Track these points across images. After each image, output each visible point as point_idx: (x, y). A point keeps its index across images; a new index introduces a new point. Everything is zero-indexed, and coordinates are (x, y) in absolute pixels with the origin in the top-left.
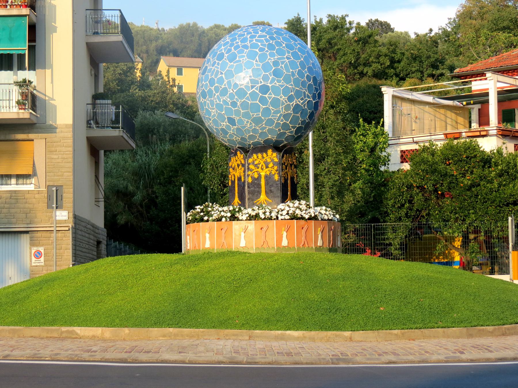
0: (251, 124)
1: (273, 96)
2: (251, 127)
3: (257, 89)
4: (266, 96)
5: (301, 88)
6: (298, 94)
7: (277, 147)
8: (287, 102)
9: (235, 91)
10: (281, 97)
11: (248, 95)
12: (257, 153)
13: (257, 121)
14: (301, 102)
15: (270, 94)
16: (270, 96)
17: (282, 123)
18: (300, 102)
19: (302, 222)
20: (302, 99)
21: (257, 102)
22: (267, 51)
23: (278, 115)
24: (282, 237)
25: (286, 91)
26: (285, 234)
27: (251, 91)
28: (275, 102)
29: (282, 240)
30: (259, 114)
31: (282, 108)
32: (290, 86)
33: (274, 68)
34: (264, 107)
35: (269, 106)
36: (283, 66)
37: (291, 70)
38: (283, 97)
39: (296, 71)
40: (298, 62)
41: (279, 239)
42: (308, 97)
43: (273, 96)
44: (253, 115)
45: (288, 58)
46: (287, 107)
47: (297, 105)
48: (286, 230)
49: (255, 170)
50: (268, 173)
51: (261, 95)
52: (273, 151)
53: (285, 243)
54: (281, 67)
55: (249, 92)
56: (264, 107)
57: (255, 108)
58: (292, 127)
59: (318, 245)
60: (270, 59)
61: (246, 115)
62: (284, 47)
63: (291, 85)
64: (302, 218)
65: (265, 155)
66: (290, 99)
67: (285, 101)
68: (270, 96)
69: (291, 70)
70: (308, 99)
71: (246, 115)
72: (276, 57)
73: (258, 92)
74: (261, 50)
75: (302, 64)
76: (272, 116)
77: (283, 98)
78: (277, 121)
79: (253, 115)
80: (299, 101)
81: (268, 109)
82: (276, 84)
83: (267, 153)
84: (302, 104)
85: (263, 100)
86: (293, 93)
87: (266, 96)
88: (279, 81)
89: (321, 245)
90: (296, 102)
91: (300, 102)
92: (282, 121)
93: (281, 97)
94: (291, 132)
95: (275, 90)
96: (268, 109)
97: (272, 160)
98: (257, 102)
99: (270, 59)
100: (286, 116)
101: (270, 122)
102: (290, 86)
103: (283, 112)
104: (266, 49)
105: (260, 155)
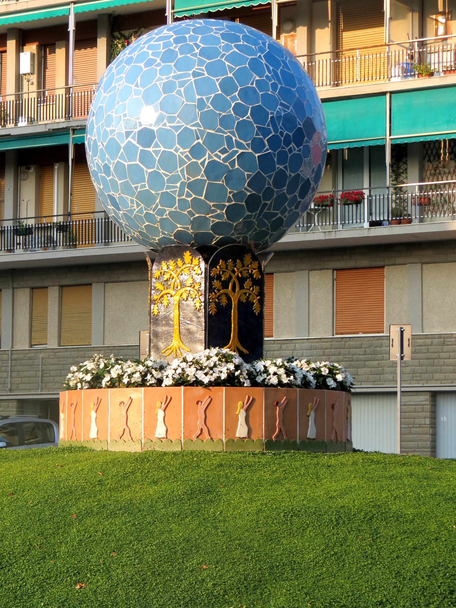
0: (138, 205)
1: (162, 149)
2: (140, 211)
3: (133, 138)
4: (150, 149)
5: (219, 130)
6: (212, 142)
7: (204, 250)
8: (189, 159)
9: (105, 144)
10: (177, 150)
11: (122, 150)
12: (167, 259)
13: (146, 198)
14: (223, 156)
15: (157, 146)
16: (156, 149)
17: (189, 199)
18: (219, 157)
19: (199, 390)
20: (223, 151)
21: (138, 162)
22: (159, 65)
23: (178, 185)
24: (156, 420)
25: (185, 137)
26: (160, 414)
27: (126, 142)
28: (168, 160)
29: (155, 427)
30: (144, 186)
31: (182, 171)
32: (194, 128)
33: (164, 95)
34: (149, 171)
35: (158, 168)
36: (182, 89)
37: (198, 97)
38: (181, 150)
39: (208, 99)
40: (217, 81)
41: (150, 426)
42: (240, 146)
43: (162, 149)
44: (136, 188)
45: (195, 74)
46: (193, 169)
47: (213, 164)
48: (163, 406)
49: (164, 292)
50: (244, 300)
51: (141, 148)
52: (193, 255)
53: (160, 431)
54: (179, 92)
55: (123, 145)
56: (149, 171)
57: (136, 174)
58: (213, 205)
59: (237, 435)
60: (159, 79)
61: (126, 188)
62: (195, 55)
63: (197, 125)
64: (198, 383)
65: (180, 262)
66: (196, 151)
67: (187, 157)
68: (156, 149)
69: (198, 97)
70: (240, 151)
71: (126, 188)
72: (172, 74)
73: (135, 143)
74: (150, 63)
75: (227, 86)
76: (168, 187)
77: (181, 152)
78: (179, 196)
79: (136, 188)
80: (216, 155)
81: (156, 174)
82: (165, 125)
83: (183, 259)
84: (225, 160)
85: (146, 158)
86: (200, 141)
87: (150, 149)
88: (171, 120)
89: (163, 435)
90: (210, 157)
91: (219, 157)
92: (189, 195)
93: (177, 150)
94: (217, 216)
95: (165, 136)
96: (156, 174)
97: (251, 275)
98: (138, 162)
99: (159, 79)
100: (194, 186)
101: (167, 199)
102: (194, 128)
103: (185, 178)
104: (158, 61)
105: (171, 263)
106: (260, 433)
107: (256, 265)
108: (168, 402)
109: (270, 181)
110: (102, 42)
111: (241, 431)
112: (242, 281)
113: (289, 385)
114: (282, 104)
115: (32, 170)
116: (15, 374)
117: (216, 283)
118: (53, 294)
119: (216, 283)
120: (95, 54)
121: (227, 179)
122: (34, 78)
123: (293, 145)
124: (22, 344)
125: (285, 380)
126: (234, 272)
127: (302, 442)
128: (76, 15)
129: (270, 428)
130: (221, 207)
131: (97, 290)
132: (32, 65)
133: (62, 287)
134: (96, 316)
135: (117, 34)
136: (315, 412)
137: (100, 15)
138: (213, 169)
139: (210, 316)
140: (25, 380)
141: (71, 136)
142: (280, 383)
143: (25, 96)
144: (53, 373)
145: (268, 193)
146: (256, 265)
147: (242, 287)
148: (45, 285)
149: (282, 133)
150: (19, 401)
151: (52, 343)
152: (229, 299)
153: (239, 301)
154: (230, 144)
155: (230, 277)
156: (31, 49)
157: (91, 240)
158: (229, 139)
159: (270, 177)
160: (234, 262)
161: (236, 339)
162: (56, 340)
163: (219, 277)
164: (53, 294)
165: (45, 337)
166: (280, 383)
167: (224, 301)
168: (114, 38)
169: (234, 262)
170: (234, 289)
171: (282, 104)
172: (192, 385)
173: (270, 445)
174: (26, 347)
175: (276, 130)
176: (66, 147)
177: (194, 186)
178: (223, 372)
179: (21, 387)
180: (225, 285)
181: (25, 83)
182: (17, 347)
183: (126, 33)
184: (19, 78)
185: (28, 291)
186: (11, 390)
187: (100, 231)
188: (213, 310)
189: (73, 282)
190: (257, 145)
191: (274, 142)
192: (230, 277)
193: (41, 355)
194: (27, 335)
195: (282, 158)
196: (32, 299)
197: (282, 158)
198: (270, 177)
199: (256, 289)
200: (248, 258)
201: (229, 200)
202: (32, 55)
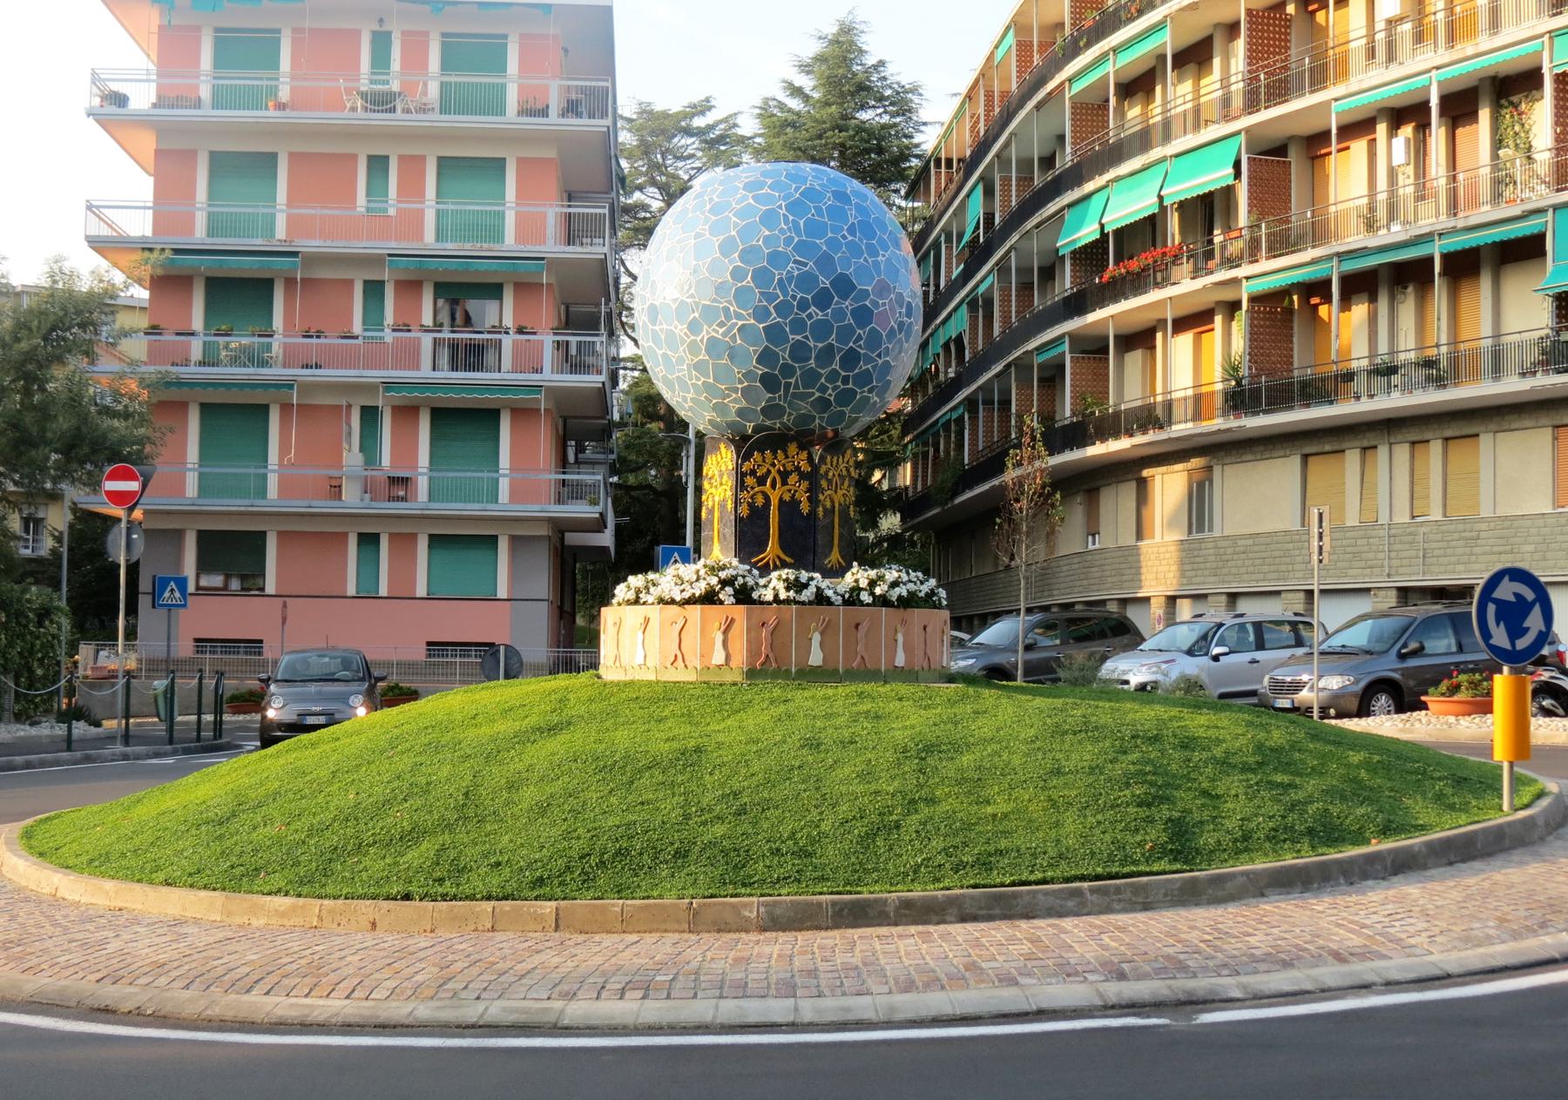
20: (721, 325)
41: (706, 654)
42: (739, 316)
46: (693, 348)
50: (787, 497)
64: (673, 602)
66: (694, 327)
77: (680, 329)
84: (724, 335)
89: (722, 661)
97: (798, 468)
100: (698, 366)
106: (740, 659)
107: (804, 455)
108: (730, 623)
109: (784, 355)
110: (1484, 114)
111: (718, 657)
112: (784, 475)
113: (788, 601)
114: (796, 262)
115: (1410, 289)
116: (1393, 554)
117: (750, 481)
118: (1436, 447)
119: (750, 481)
120: (1477, 132)
121: (731, 357)
122: (1410, 170)
123: (813, 309)
124: (1403, 517)
125: (783, 595)
126: (773, 465)
127: (847, 672)
128: (1439, 82)
129: (753, 652)
130: (735, 390)
131: (1485, 440)
132: (1408, 153)
133: (1447, 439)
134: (1486, 477)
135: (1503, 102)
136: (822, 633)
137: (1481, 80)
138: (712, 344)
139: (742, 519)
140: (1405, 562)
141: (1437, 243)
142: (776, 600)
143: (1401, 192)
144: (1436, 552)
145: (787, 370)
146: (804, 455)
147: (784, 483)
148: (1373, 443)
149: (794, 297)
150: (1399, 589)
151: (1436, 514)
152: (767, 498)
153: (781, 499)
154: (728, 317)
155: (769, 472)
156: (1407, 131)
157: (1475, 375)
158: (726, 310)
159: (784, 351)
160: (774, 453)
161: (777, 546)
162: (1440, 511)
163: (753, 473)
164: (1436, 447)
165: (1428, 506)
166: (776, 600)
167: (760, 501)
168: (1501, 106)
169: (774, 453)
170: (773, 486)
171: (796, 262)
172: (667, 603)
173: (751, 674)
174: (1407, 519)
175: (785, 293)
176: (1430, 259)
177: (698, 366)
178: (699, 589)
179: (1401, 570)
180: (761, 481)
181: (1401, 177)
182: (1396, 520)
183: (1515, 99)
184: (1392, 173)
185: (1406, 447)
186: (1389, 575)
187: (1486, 362)
188: (744, 511)
189: (1457, 433)
190: (761, 314)
191: (782, 309)
192: (769, 472)
193: (1423, 529)
194: (1407, 504)
195: (798, 326)
196: (1412, 456)
197: (798, 326)
198: (784, 351)
199: (805, 485)
200: (793, 448)
201: (740, 382)
202: (1408, 140)
